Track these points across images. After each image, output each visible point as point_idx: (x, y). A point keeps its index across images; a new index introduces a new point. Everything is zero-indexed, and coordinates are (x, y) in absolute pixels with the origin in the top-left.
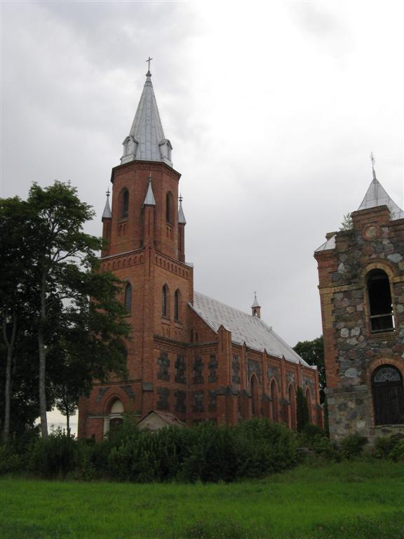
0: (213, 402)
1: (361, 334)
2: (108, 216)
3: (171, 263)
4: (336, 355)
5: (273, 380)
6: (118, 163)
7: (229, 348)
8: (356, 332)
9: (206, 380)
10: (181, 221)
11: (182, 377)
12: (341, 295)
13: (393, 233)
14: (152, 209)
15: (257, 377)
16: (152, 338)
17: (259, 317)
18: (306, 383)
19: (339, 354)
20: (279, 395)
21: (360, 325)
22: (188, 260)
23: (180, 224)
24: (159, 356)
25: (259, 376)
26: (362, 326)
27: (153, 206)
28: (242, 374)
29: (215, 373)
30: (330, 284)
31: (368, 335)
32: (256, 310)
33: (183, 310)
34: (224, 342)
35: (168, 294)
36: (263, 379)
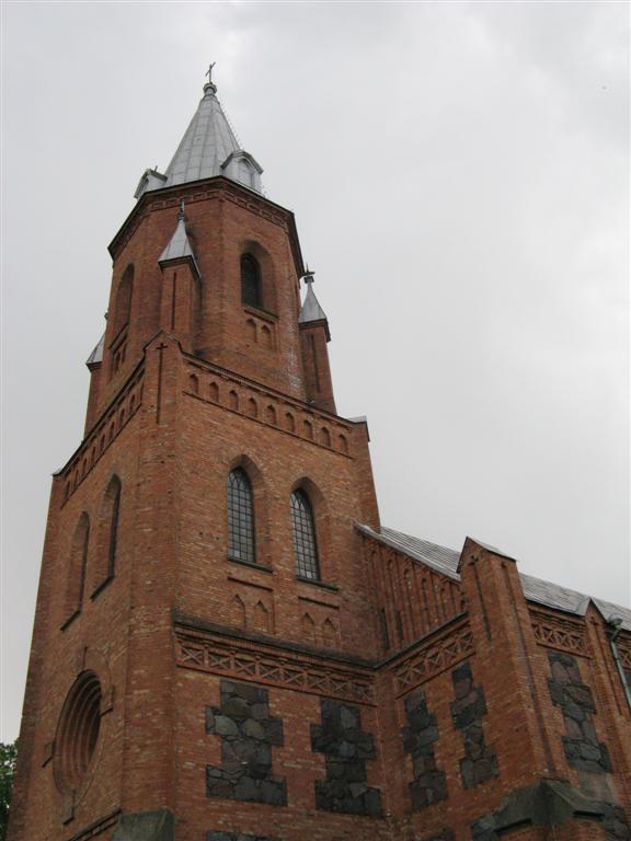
2: (99, 358)
6: (521, 568)
9: (454, 775)
11: (357, 790)
14: (186, 268)
16: (164, 625)
22: (346, 408)
23: (304, 326)
24: (216, 701)
33: (338, 543)
34: (488, 599)
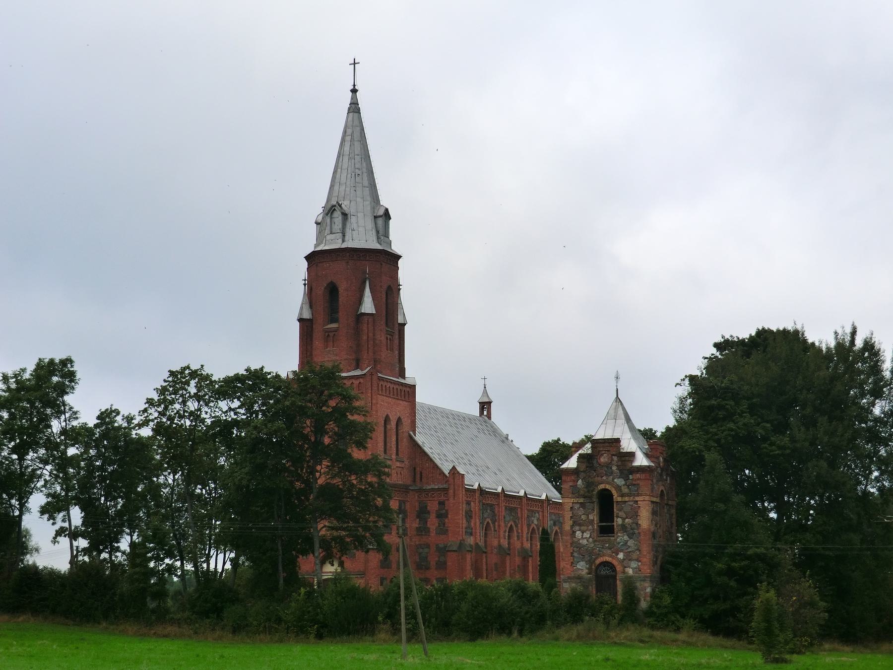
0: (442, 559)
1: (590, 537)
3: (392, 386)
4: (572, 551)
5: (511, 525)
7: (461, 494)
8: (587, 535)
10: (400, 320)
12: (578, 506)
13: (620, 462)
15: (491, 525)
17: (489, 417)
18: (555, 524)
19: (573, 550)
20: (518, 545)
21: (590, 530)
25: (494, 523)
26: (591, 531)
27: (372, 314)
28: (475, 524)
29: (444, 524)
30: (570, 496)
31: (595, 538)
32: (485, 406)
35: (388, 426)
36: (499, 526)
